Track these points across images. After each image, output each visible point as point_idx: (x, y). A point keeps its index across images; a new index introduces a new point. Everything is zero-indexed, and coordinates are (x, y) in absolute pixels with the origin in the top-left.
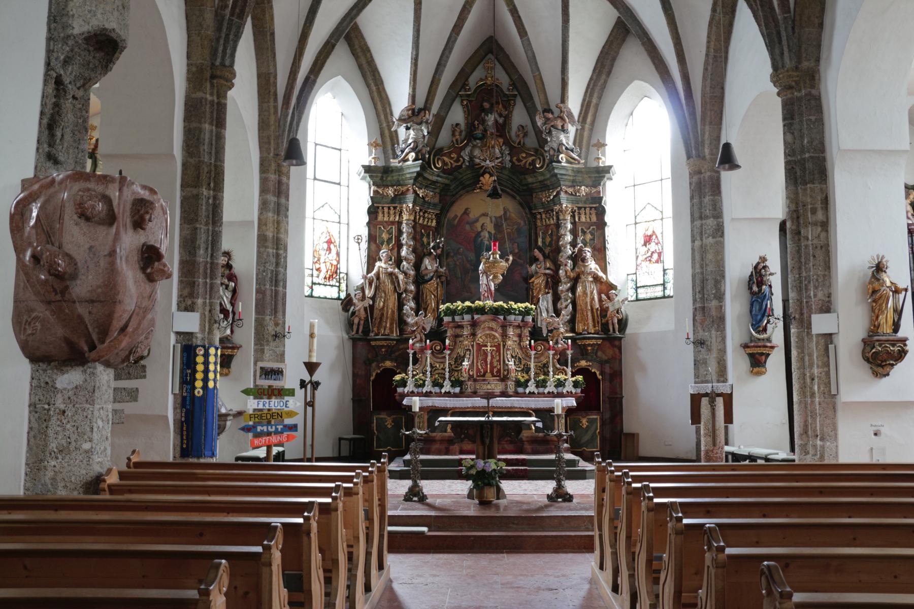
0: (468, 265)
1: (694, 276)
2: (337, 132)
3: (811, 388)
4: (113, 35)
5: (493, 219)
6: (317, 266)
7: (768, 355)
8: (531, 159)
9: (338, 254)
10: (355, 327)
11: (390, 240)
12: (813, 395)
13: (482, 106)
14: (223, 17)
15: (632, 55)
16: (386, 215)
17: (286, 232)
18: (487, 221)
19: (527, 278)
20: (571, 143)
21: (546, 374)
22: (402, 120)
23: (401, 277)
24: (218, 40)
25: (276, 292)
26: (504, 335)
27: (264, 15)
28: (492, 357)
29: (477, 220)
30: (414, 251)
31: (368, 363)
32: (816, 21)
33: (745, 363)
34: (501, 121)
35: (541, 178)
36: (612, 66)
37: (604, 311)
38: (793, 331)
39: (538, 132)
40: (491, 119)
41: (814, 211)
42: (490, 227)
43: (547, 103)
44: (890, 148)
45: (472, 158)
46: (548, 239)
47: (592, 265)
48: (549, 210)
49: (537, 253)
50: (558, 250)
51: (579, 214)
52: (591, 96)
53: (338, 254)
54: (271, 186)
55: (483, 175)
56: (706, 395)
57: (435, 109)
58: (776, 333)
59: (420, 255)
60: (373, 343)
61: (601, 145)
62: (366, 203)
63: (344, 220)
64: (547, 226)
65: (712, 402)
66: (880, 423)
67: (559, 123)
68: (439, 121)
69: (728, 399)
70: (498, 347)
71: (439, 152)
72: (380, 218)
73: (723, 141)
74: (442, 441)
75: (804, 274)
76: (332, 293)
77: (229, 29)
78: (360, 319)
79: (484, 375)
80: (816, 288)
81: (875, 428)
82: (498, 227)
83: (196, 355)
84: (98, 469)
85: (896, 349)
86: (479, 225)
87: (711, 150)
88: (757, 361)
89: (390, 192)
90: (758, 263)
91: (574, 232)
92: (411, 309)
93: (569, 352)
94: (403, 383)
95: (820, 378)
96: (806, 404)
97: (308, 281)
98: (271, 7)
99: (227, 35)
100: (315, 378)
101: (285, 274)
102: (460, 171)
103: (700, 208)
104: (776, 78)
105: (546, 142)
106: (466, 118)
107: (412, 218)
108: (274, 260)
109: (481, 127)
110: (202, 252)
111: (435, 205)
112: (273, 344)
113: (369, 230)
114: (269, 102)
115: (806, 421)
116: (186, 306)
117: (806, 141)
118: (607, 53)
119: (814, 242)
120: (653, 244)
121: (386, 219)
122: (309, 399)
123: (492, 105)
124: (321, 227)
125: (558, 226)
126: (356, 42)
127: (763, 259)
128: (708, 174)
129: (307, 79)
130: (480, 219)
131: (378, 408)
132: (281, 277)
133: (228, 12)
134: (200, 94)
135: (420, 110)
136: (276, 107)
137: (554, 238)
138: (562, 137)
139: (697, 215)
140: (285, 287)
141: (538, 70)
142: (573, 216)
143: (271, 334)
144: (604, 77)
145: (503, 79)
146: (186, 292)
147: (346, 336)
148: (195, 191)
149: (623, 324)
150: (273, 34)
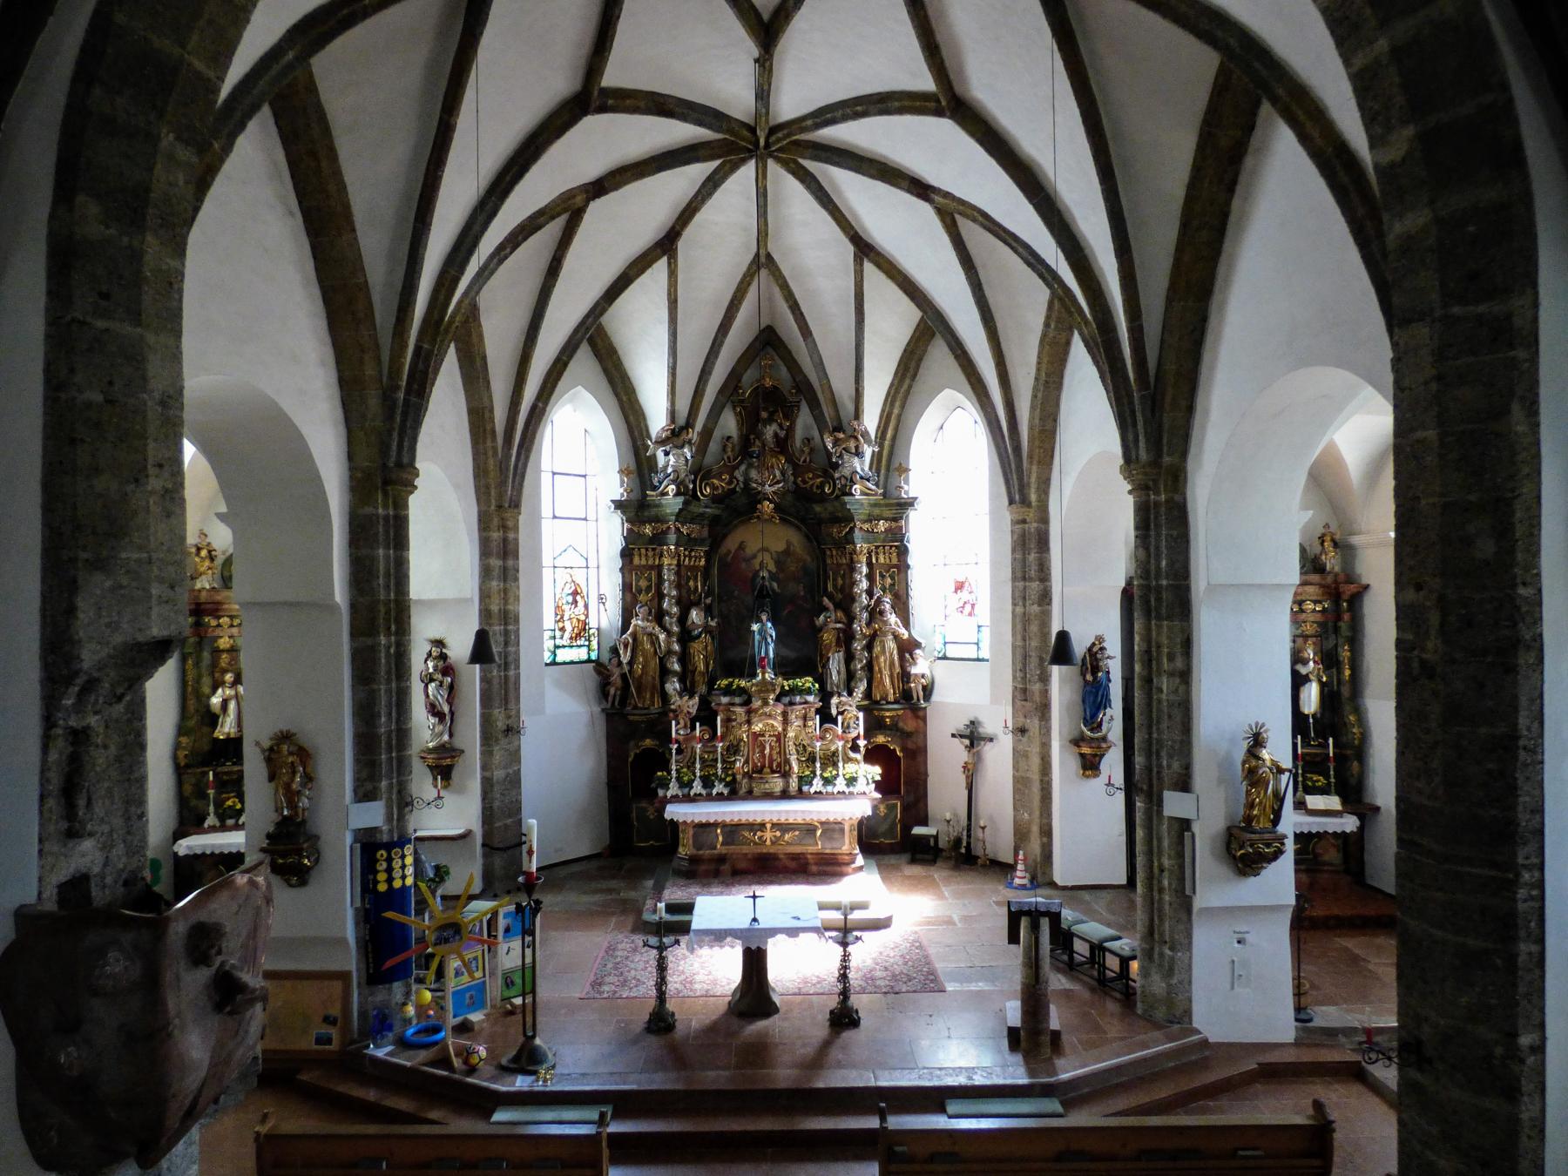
1: (1014, 647)
2: (578, 458)
3: (1160, 882)
9: (586, 606)
11: (648, 589)
12: (1161, 890)
14: (394, 402)
17: (517, 598)
20: (867, 468)
21: (835, 765)
23: (662, 637)
28: (771, 748)
29: (755, 556)
30: (678, 603)
33: (1074, 764)
37: (905, 676)
40: (770, 431)
41: (1171, 658)
44: (1275, 581)
45: (747, 481)
47: (893, 619)
50: (852, 598)
53: (586, 606)
55: (760, 502)
56: (1028, 913)
59: (685, 606)
62: (618, 543)
64: (839, 565)
65: (1035, 927)
66: (1245, 929)
67: (852, 444)
68: (707, 434)
72: (636, 561)
73: (1055, 629)
76: (582, 654)
77: (405, 414)
80: (1170, 757)
82: (778, 563)
88: (1090, 765)
89: (648, 530)
91: (870, 577)
95: (1171, 872)
97: (549, 644)
98: (480, 325)
99: (404, 421)
106: (740, 429)
115: (1152, 920)
116: (365, 794)
117: (1164, 563)
119: (1172, 697)
121: (643, 562)
123: (772, 414)
125: (852, 568)
127: (1100, 639)
129: (534, 408)
134: (368, 510)
136: (495, 449)
138: (856, 462)
139: (1019, 575)
142: (869, 558)
144: (907, 381)
146: (364, 775)
147: (597, 709)
148: (369, 641)
149: (928, 691)
150: (484, 358)
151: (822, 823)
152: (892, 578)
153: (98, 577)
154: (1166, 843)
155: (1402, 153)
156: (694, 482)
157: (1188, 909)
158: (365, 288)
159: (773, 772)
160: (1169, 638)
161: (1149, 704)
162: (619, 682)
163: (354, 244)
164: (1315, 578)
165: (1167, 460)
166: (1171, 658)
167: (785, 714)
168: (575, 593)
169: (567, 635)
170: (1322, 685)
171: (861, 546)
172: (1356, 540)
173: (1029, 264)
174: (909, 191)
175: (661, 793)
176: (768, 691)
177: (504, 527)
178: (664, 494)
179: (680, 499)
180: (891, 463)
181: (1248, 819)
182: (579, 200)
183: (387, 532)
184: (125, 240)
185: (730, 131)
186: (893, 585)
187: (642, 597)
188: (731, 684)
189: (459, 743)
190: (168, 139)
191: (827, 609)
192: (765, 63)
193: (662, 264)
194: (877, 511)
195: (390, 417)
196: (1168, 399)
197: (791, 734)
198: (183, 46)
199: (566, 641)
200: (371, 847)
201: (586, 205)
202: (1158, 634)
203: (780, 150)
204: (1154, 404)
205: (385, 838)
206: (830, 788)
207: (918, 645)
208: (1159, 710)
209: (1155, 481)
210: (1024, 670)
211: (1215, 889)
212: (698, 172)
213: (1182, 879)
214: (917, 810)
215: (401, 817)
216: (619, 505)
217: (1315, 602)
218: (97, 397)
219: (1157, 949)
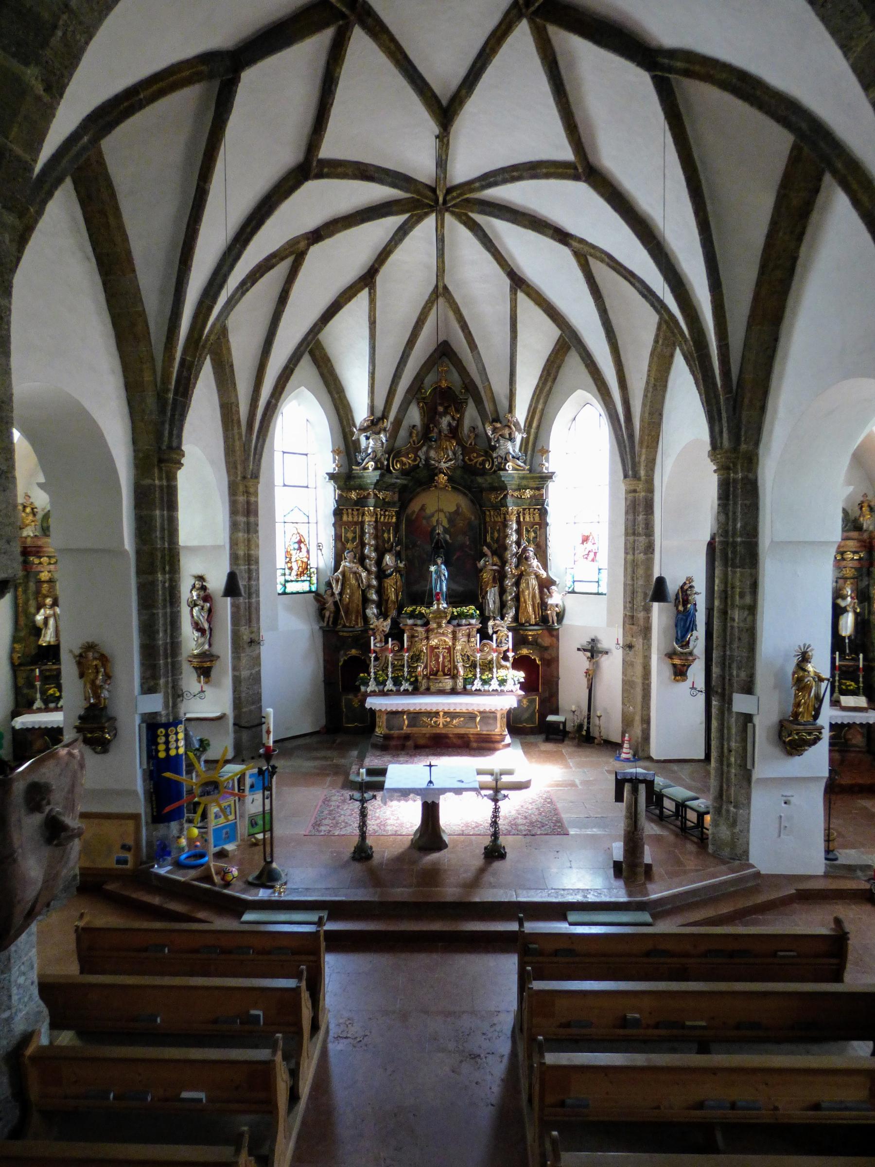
0: (425, 556)
1: (625, 585)
2: (302, 445)
3: (728, 759)
5: (447, 514)
6: (289, 565)
8: (481, 459)
9: (308, 552)
10: (326, 620)
11: (354, 539)
13: (436, 408)
16: (350, 516)
17: (257, 546)
18: (442, 516)
20: (517, 450)
21: (491, 670)
22: (363, 430)
23: (364, 575)
25: (250, 603)
26: (455, 638)
27: (221, 350)
28: (444, 657)
29: (433, 515)
30: (376, 550)
32: (758, 404)
33: (668, 672)
34: (454, 424)
36: (557, 372)
37: (544, 605)
38: (714, 703)
41: (742, 595)
42: (445, 523)
43: (496, 411)
44: (822, 540)
45: (427, 459)
47: (535, 563)
49: (485, 549)
50: (505, 548)
51: (524, 514)
53: (308, 552)
54: (240, 507)
55: (436, 475)
56: (630, 781)
57: (392, 417)
60: (341, 634)
61: (545, 451)
62: (331, 505)
63: (312, 520)
64: (495, 522)
65: (635, 791)
67: (506, 432)
68: (398, 423)
72: (345, 518)
73: (656, 575)
74: (399, 738)
75: (728, 653)
76: (305, 587)
77: (174, 409)
78: (331, 612)
80: (739, 668)
81: (785, 798)
82: (451, 521)
84: (19, 1026)
86: (434, 519)
87: (647, 471)
88: (680, 673)
89: (353, 495)
90: (685, 584)
91: (519, 532)
94: (367, 684)
95: (736, 751)
97: (280, 579)
98: (228, 341)
99: (173, 415)
102: (418, 470)
103: (634, 525)
106: (422, 420)
107: (374, 519)
108: (246, 575)
109: (436, 430)
110: (161, 635)
112: (248, 650)
114: (233, 430)
116: (149, 688)
117: (739, 525)
118: (552, 362)
119: (742, 625)
120: (590, 543)
121: (350, 519)
123: (446, 408)
124: (291, 529)
125: (505, 525)
127: (690, 579)
128: (643, 494)
129: (269, 403)
130: (436, 515)
134: (147, 482)
136: (240, 434)
137: (501, 535)
139: (630, 531)
141: (488, 381)
142: (518, 517)
148: (150, 578)
149: (560, 616)
150: (232, 366)
152: (535, 533)
154: (734, 731)
156: (388, 460)
158: (142, 314)
159: (445, 675)
162: (332, 608)
164: (855, 534)
165: (743, 447)
166: (742, 595)
167: (454, 633)
168: (300, 542)
169: (294, 573)
170: (857, 615)
171: (512, 508)
173: (644, 296)
175: (363, 688)
176: (441, 617)
177: (247, 493)
178: (365, 468)
179: (378, 473)
180: (535, 447)
181: (796, 715)
183: (162, 498)
186: (535, 538)
189: (215, 650)
191: (485, 555)
193: (365, 294)
194: (524, 482)
196: (746, 401)
197: (458, 647)
198: (7, 138)
200: (153, 727)
201: (307, 249)
204: (736, 405)
205: (164, 720)
206: (486, 687)
207: (553, 583)
208: (732, 634)
209: (735, 465)
210: (632, 602)
211: (768, 764)
212: (393, 222)
213: (744, 758)
214: (550, 703)
216: (332, 476)
217: (854, 553)
219: (724, 807)
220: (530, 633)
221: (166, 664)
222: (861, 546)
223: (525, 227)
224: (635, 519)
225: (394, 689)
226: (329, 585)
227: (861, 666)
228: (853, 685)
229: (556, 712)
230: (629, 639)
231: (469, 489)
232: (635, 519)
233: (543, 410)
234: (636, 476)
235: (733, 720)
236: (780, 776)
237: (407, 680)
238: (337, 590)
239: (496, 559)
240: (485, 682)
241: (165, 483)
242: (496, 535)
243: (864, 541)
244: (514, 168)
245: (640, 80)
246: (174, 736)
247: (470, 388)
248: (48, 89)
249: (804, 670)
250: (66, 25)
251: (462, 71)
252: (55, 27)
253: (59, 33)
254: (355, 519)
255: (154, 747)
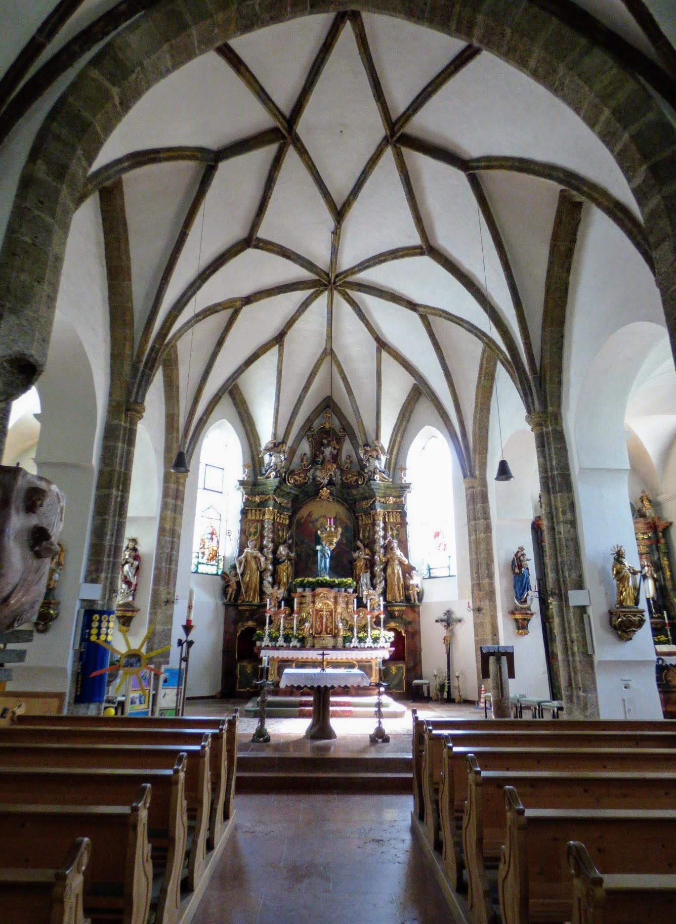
1: (471, 561)
2: (221, 455)
3: (572, 649)
4: (31, 360)
7: (529, 620)
9: (218, 542)
11: (256, 533)
12: (573, 654)
15: (424, 408)
17: (180, 525)
19: (352, 562)
20: (383, 467)
21: (366, 632)
22: (267, 450)
23: (263, 559)
24: (133, 384)
25: (170, 569)
26: (336, 602)
29: (317, 520)
30: (273, 541)
31: (236, 623)
33: (512, 627)
35: (362, 491)
36: (410, 416)
37: (406, 587)
39: (360, 460)
40: (328, 451)
45: (314, 479)
46: (367, 534)
47: (398, 552)
48: (367, 513)
49: (359, 543)
50: (374, 542)
52: (396, 436)
53: (218, 542)
54: (171, 492)
56: (493, 654)
57: (290, 442)
58: (534, 605)
60: (240, 608)
64: (366, 524)
65: (498, 661)
67: (375, 454)
68: (293, 451)
69: (510, 656)
70: (331, 612)
71: (292, 473)
72: (249, 517)
75: (559, 560)
76: (212, 570)
79: (320, 633)
80: (570, 570)
83: (92, 621)
85: (637, 619)
91: (385, 529)
92: (269, 582)
93: (382, 617)
94: (261, 639)
95: (578, 641)
96: (568, 661)
97: (195, 561)
98: (178, 369)
99: (141, 382)
100: (190, 638)
101: (177, 557)
104: (529, 419)
105: (365, 466)
106: (311, 451)
108: (169, 545)
110: (108, 537)
111: (288, 509)
113: (241, 526)
115: (570, 676)
116: (92, 577)
117: (554, 463)
119: (567, 535)
121: (253, 518)
122: (184, 655)
123: (329, 442)
125: (374, 524)
126: (237, 396)
127: (522, 549)
129: (201, 419)
131: (242, 658)
132: (174, 558)
133: (142, 365)
134: (116, 422)
135: (280, 443)
136: (177, 438)
138: (377, 463)
139: (472, 517)
140: (177, 566)
142: (384, 518)
143: (163, 601)
145: (336, 423)
146: (93, 568)
147: (221, 603)
148: (106, 491)
149: (420, 595)
150: (178, 388)
151: (358, 662)
152: (398, 530)
153: (13, 317)
154: (573, 624)
155: (643, 178)
156: (285, 473)
157: (591, 665)
158: (131, 309)
159: (327, 634)
160: (561, 502)
161: (554, 542)
162: (235, 586)
163: (129, 287)
164: (642, 520)
165: (550, 409)
166: (564, 513)
167: (336, 598)
168: (212, 534)
169: (206, 557)
170: (655, 580)
171: (380, 510)
172: (660, 498)
173: (470, 331)
174: (406, 307)
175: (258, 643)
176: (333, 536)
177: (177, 482)
178: (268, 477)
179: (277, 480)
180: (396, 466)
181: (621, 603)
182: (238, 304)
183: (125, 435)
184: (55, 184)
185: (317, 274)
186: (398, 535)
187: (251, 538)
188: (302, 581)
189: (137, 604)
190: (80, 152)
191: (359, 548)
192: (336, 234)
193: (276, 348)
194: (388, 492)
195: (134, 376)
196: (548, 378)
197: (339, 610)
198: (94, 117)
199: (204, 561)
200: (91, 614)
201: (241, 308)
202: (555, 501)
203: (340, 285)
204: (540, 381)
205: (99, 608)
206: (362, 644)
207: (414, 569)
208: (560, 544)
209: (545, 421)
210: (478, 572)
211: (606, 649)
212: (300, 296)
213: (585, 645)
214: (415, 670)
215: (110, 599)
216: (242, 483)
217: (643, 534)
218: (28, 239)
219: (575, 694)
220: (396, 608)
221: (109, 562)
222: (648, 528)
223: (388, 300)
224: (474, 509)
225: (285, 645)
226: (234, 567)
227: (667, 621)
228: (663, 638)
229: (421, 678)
230: (478, 603)
231: (346, 501)
232: (474, 509)
233: (400, 442)
234: (473, 476)
235: (571, 614)
236: (617, 659)
237: (296, 637)
238: (239, 571)
239: (367, 551)
240: (361, 640)
241: (128, 425)
242: (367, 534)
243: (649, 523)
244: (381, 255)
245: (459, 177)
246: (106, 624)
247: (347, 430)
248: (121, 103)
249: (621, 563)
250: (138, 73)
251: (351, 186)
252: (133, 71)
253: (134, 76)
254: (258, 518)
255: (87, 631)
